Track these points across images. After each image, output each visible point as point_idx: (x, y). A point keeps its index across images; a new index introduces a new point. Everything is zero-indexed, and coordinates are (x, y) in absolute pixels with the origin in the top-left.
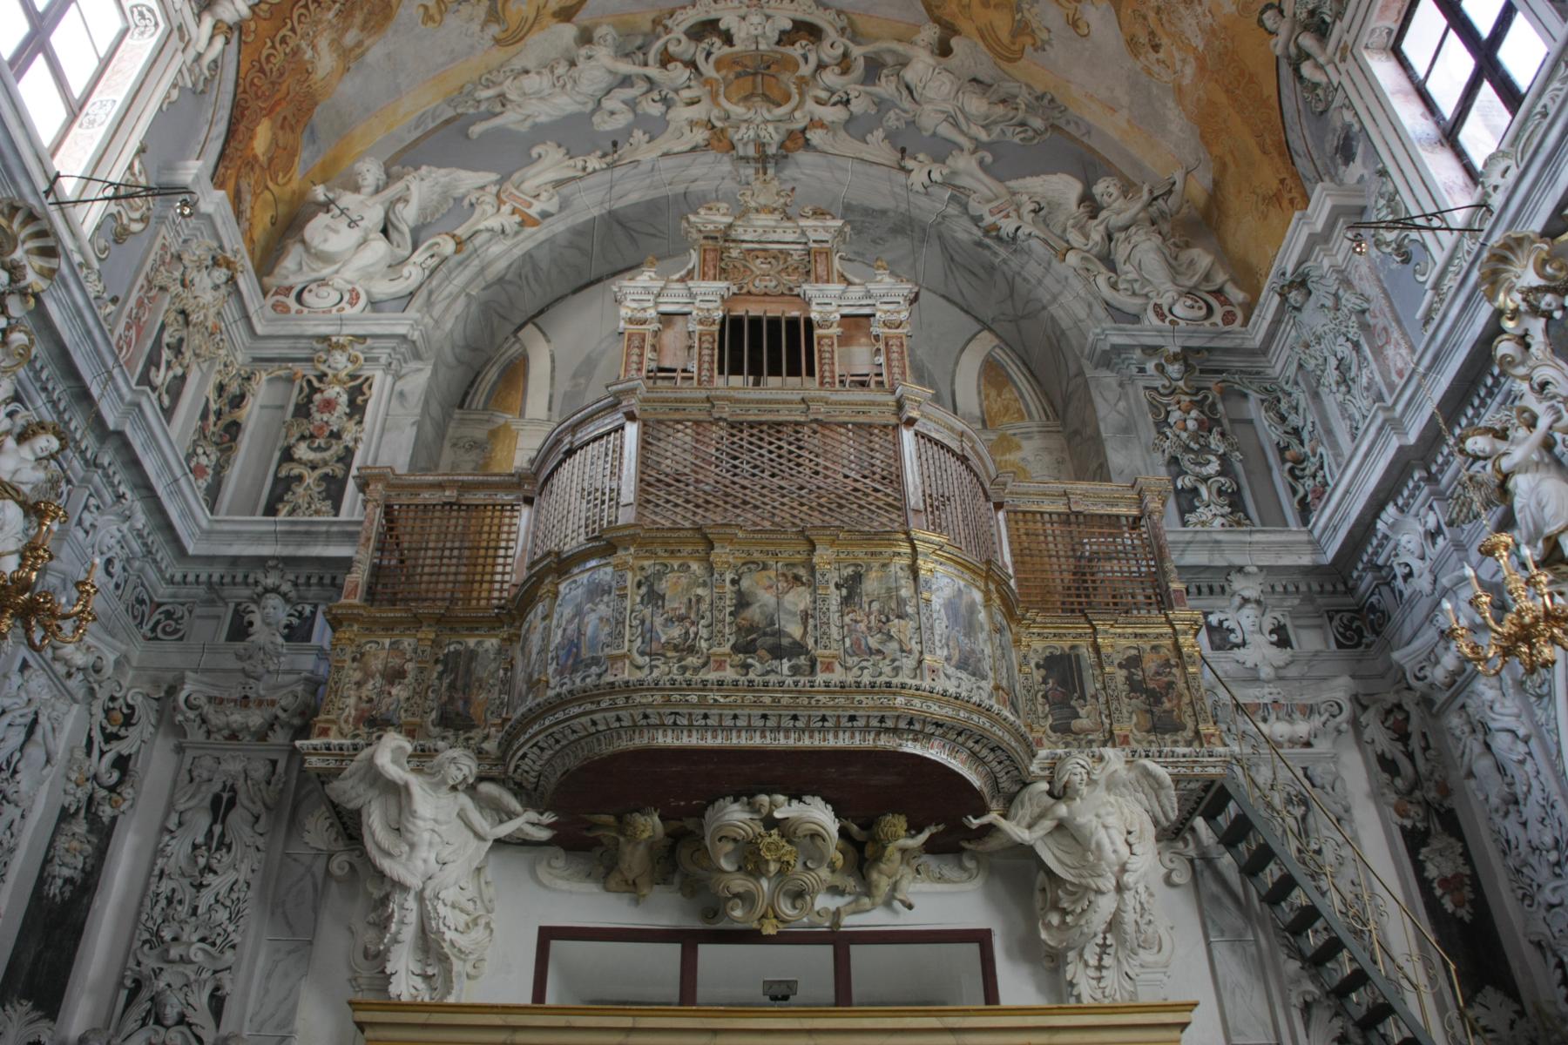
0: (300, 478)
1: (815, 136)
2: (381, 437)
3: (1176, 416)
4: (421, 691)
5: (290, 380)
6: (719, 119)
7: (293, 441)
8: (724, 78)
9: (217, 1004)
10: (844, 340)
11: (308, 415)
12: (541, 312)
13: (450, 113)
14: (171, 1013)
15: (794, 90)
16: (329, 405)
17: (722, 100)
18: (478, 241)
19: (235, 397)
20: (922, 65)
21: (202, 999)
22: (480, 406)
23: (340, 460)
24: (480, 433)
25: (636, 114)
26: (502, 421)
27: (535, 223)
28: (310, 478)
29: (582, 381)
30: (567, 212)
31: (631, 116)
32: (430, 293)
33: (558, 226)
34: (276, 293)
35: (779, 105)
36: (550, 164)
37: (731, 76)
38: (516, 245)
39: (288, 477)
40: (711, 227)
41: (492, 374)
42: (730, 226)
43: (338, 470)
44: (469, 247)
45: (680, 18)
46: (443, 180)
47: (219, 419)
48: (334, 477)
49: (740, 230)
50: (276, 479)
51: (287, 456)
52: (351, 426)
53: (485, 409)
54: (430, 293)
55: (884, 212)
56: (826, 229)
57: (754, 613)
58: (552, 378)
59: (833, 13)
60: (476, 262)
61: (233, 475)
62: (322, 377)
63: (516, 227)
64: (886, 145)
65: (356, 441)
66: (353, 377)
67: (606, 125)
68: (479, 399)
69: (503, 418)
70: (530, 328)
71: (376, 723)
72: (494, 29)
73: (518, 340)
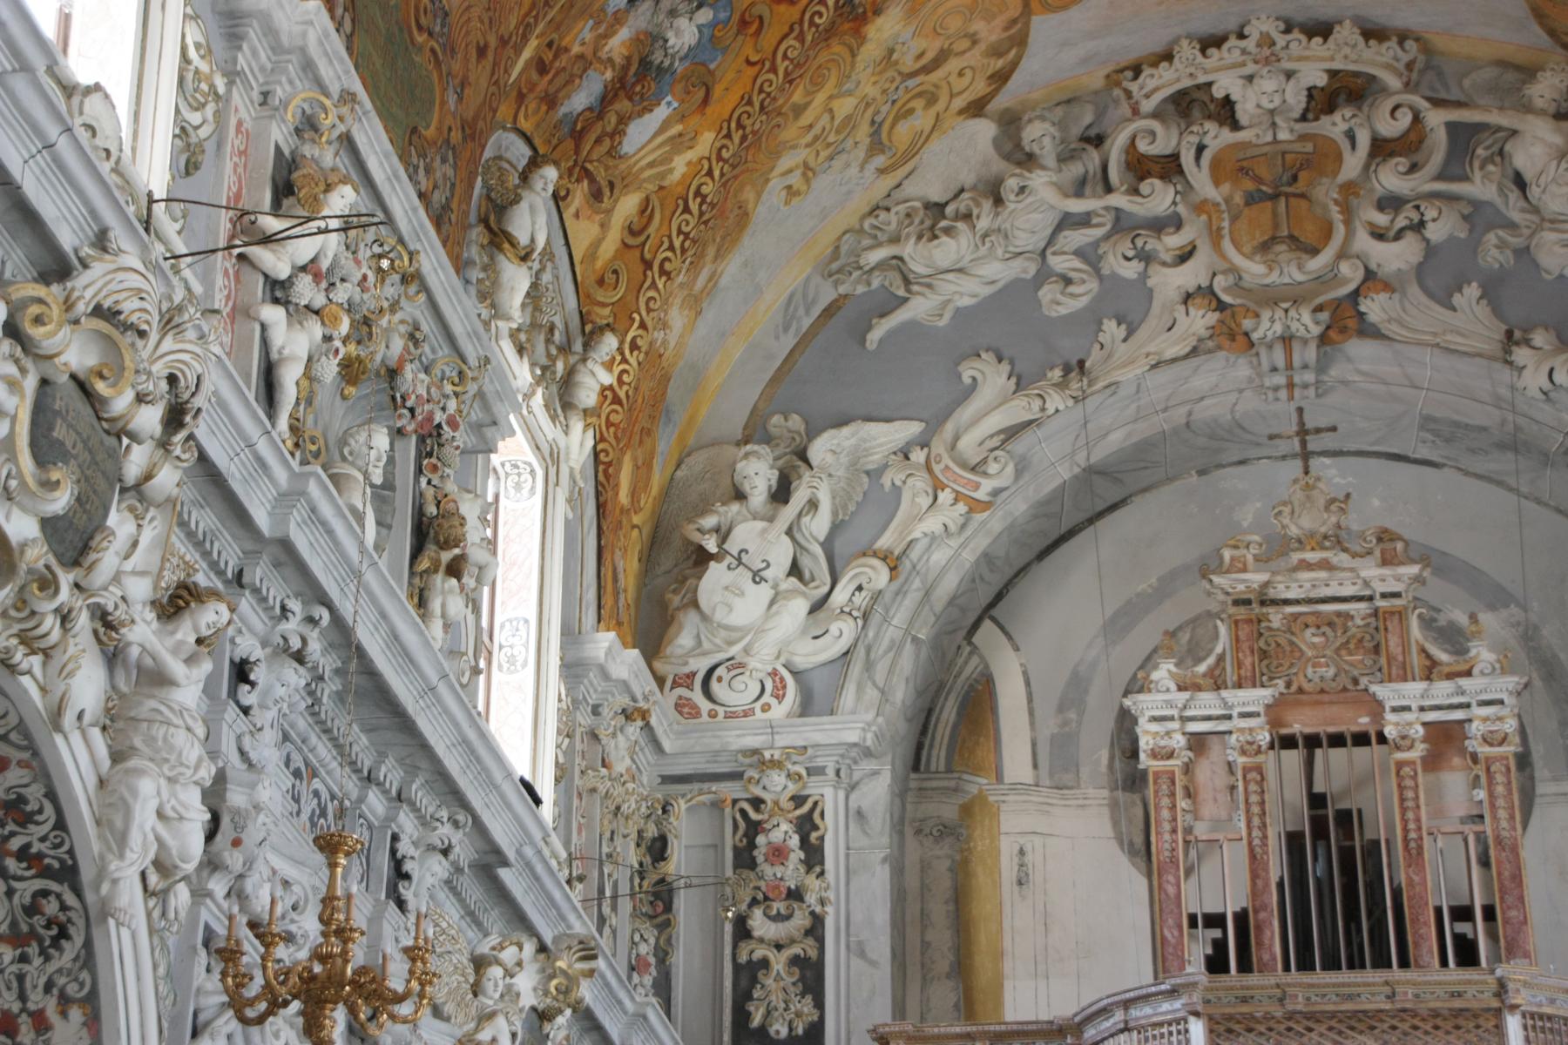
0: (765, 963)
1: (1375, 307)
2: (848, 883)
5: (717, 805)
6: (1226, 290)
7: (744, 907)
8: (1227, 200)
10: (1433, 762)
11: (752, 865)
12: (999, 597)
13: (827, 295)
16: (778, 854)
17: (1227, 245)
18: (914, 554)
19: (654, 840)
22: (942, 768)
23: (809, 932)
24: (948, 811)
25: (1101, 278)
26: (974, 790)
27: (986, 506)
28: (779, 962)
29: (1072, 715)
30: (1026, 477)
31: (1093, 285)
32: (868, 650)
33: (1019, 506)
34: (675, 684)
35: (1314, 252)
37: (1238, 199)
38: (963, 546)
39: (750, 962)
40: (1241, 587)
41: (948, 712)
42: (1266, 584)
43: (808, 948)
44: (906, 565)
45: (1151, 84)
46: (847, 443)
47: (642, 879)
48: (807, 959)
49: (1281, 587)
50: (737, 967)
51: (742, 931)
52: (812, 882)
53: (949, 770)
54: (868, 650)
55: (1484, 429)
56: (1398, 579)
58: (1031, 713)
59: (1393, 43)
60: (917, 583)
61: (680, 961)
62: (757, 803)
63: (961, 520)
64: (1483, 311)
65: (822, 902)
66: (798, 800)
67: (1057, 303)
68: (938, 756)
69: (977, 784)
70: (987, 624)
72: (880, 161)
73: (975, 649)
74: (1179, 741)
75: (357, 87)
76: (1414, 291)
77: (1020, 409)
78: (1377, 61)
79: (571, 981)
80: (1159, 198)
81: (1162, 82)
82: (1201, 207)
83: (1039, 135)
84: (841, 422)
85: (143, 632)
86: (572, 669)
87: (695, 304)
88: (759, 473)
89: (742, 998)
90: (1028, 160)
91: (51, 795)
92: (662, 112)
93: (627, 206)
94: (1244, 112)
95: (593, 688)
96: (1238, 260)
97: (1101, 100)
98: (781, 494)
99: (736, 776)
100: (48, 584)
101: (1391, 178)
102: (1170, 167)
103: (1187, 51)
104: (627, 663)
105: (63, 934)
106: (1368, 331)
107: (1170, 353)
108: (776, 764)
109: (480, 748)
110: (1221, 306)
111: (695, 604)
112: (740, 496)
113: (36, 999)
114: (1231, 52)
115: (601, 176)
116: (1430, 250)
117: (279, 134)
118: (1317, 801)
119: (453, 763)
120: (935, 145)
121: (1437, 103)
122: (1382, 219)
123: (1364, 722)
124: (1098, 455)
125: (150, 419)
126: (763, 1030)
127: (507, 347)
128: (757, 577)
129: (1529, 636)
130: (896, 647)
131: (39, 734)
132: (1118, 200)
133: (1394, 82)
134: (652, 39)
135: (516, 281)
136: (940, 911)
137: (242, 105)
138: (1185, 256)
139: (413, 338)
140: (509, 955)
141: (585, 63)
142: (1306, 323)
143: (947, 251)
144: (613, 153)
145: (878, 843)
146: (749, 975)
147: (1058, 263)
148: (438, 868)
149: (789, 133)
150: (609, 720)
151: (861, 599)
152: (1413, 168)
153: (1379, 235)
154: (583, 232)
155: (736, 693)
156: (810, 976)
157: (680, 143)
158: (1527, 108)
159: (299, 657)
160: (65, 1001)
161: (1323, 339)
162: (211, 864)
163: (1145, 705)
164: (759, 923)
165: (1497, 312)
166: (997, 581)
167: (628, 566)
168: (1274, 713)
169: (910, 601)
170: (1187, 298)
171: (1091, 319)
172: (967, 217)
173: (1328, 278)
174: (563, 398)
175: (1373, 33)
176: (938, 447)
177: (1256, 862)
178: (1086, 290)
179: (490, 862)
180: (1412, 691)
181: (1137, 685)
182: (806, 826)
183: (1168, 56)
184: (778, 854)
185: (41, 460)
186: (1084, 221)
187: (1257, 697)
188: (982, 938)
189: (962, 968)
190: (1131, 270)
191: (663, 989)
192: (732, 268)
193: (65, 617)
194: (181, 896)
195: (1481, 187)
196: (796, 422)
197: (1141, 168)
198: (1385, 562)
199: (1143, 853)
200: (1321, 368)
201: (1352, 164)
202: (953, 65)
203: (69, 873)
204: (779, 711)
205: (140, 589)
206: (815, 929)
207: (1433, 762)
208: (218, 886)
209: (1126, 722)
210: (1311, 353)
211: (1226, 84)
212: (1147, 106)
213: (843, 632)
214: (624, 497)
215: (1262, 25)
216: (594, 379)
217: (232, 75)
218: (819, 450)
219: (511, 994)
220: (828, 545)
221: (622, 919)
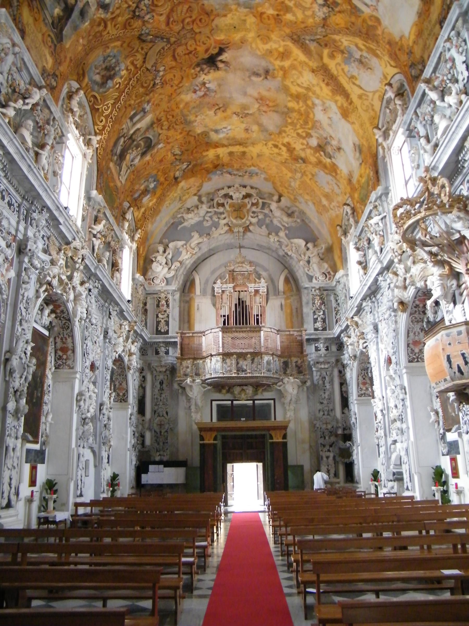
1: (251, 228)
3: (316, 302)
4: (192, 369)
9: (167, 413)
10: (255, 295)
12: (196, 267)
13: (172, 221)
14: (161, 415)
15: (246, 214)
16: (163, 305)
20: (274, 206)
21: (165, 413)
24: (188, 299)
27: (194, 254)
28: (163, 321)
33: (199, 254)
35: (243, 219)
36: (196, 239)
41: (188, 284)
43: (167, 319)
51: (157, 316)
52: (168, 310)
57: (239, 365)
61: (148, 320)
62: (160, 298)
64: (266, 230)
66: (166, 297)
67: (206, 224)
68: (186, 291)
69: (192, 295)
70: (194, 272)
71: (186, 375)
74: (220, 291)
75: (106, 206)
76: (257, 226)
77: (200, 240)
78: (253, 192)
79: (134, 327)
80: (221, 209)
81: (222, 192)
82: (227, 211)
83: (204, 199)
84: (173, 241)
85: (79, 288)
86: (133, 279)
87: (152, 224)
88: (161, 249)
89: (157, 326)
90: (202, 202)
91: (67, 310)
92: (148, 196)
93: (143, 210)
94: (234, 198)
95: (136, 282)
96: (232, 220)
97: (213, 194)
98: (164, 252)
99: (157, 294)
100: (67, 284)
101: (254, 209)
102: (223, 205)
103: (226, 188)
104: (141, 278)
105: (68, 328)
106: (250, 231)
107: (222, 232)
108: (163, 292)
109: (121, 296)
110: (229, 226)
111: (151, 268)
112: (158, 252)
113: (65, 336)
114: (232, 189)
115: (139, 206)
116: (259, 220)
117: (95, 213)
118: (239, 299)
119: (117, 299)
120: (189, 200)
121: (261, 198)
122: (252, 215)
123: (246, 289)
124: (211, 248)
125: (80, 261)
126: (160, 331)
127: (125, 233)
128: (161, 265)
129: (270, 276)
130: (181, 275)
131: (65, 302)
132: (215, 209)
133: (255, 195)
134: (148, 186)
135: (126, 225)
136: (186, 313)
137: (90, 210)
138: (225, 218)
139: (112, 237)
140: (125, 323)
141: (137, 190)
142: (241, 230)
143: (190, 216)
144: (141, 202)
145: (177, 304)
146: (158, 323)
147: (207, 218)
148: (115, 313)
149: (167, 198)
150: (139, 286)
151: (176, 268)
152: (257, 208)
153: (252, 217)
154: (136, 214)
155: (157, 281)
156: (167, 323)
157: (150, 201)
158: (272, 200)
159: (98, 288)
160: (69, 336)
161: (244, 232)
162: (87, 317)
163: (216, 286)
164: (160, 316)
165: (268, 229)
166: (196, 265)
167: (141, 262)
168: (234, 288)
169: (183, 268)
170: (225, 225)
171: (210, 228)
172: (193, 211)
173: (245, 223)
174: (132, 238)
175: (252, 188)
176: (188, 245)
177: (230, 309)
178: (210, 223)
179: (122, 311)
180: (253, 285)
181: (215, 283)
182: (167, 301)
183: (223, 189)
184: (163, 305)
185: (66, 268)
186: (210, 212)
187: (232, 285)
188: (192, 317)
189: (189, 321)
190: (217, 220)
191: (146, 324)
192: (158, 218)
193: (69, 289)
194: (83, 321)
195: (266, 211)
196: (167, 240)
197: (219, 205)
198: (250, 266)
199: (214, 305)
200: (243, 236)
201: (249, 206)
202: (192, 189)
203: (69, 320)
204: (163, 284)
205: (78, 282)
206: (168, 316)
207: (255, 295)
208: (88, 320)
209: (213, 288)
210: (242, 234)
211: (231, 193)
212: (220, 196)
213: (172, 273)
214: (141, 252)
215: (237, 185)
216: (137, 236)
217: (89, 206)
218: (171, 245)
219: (125, 329)
220: (171, 260)
221: (140, 315)
